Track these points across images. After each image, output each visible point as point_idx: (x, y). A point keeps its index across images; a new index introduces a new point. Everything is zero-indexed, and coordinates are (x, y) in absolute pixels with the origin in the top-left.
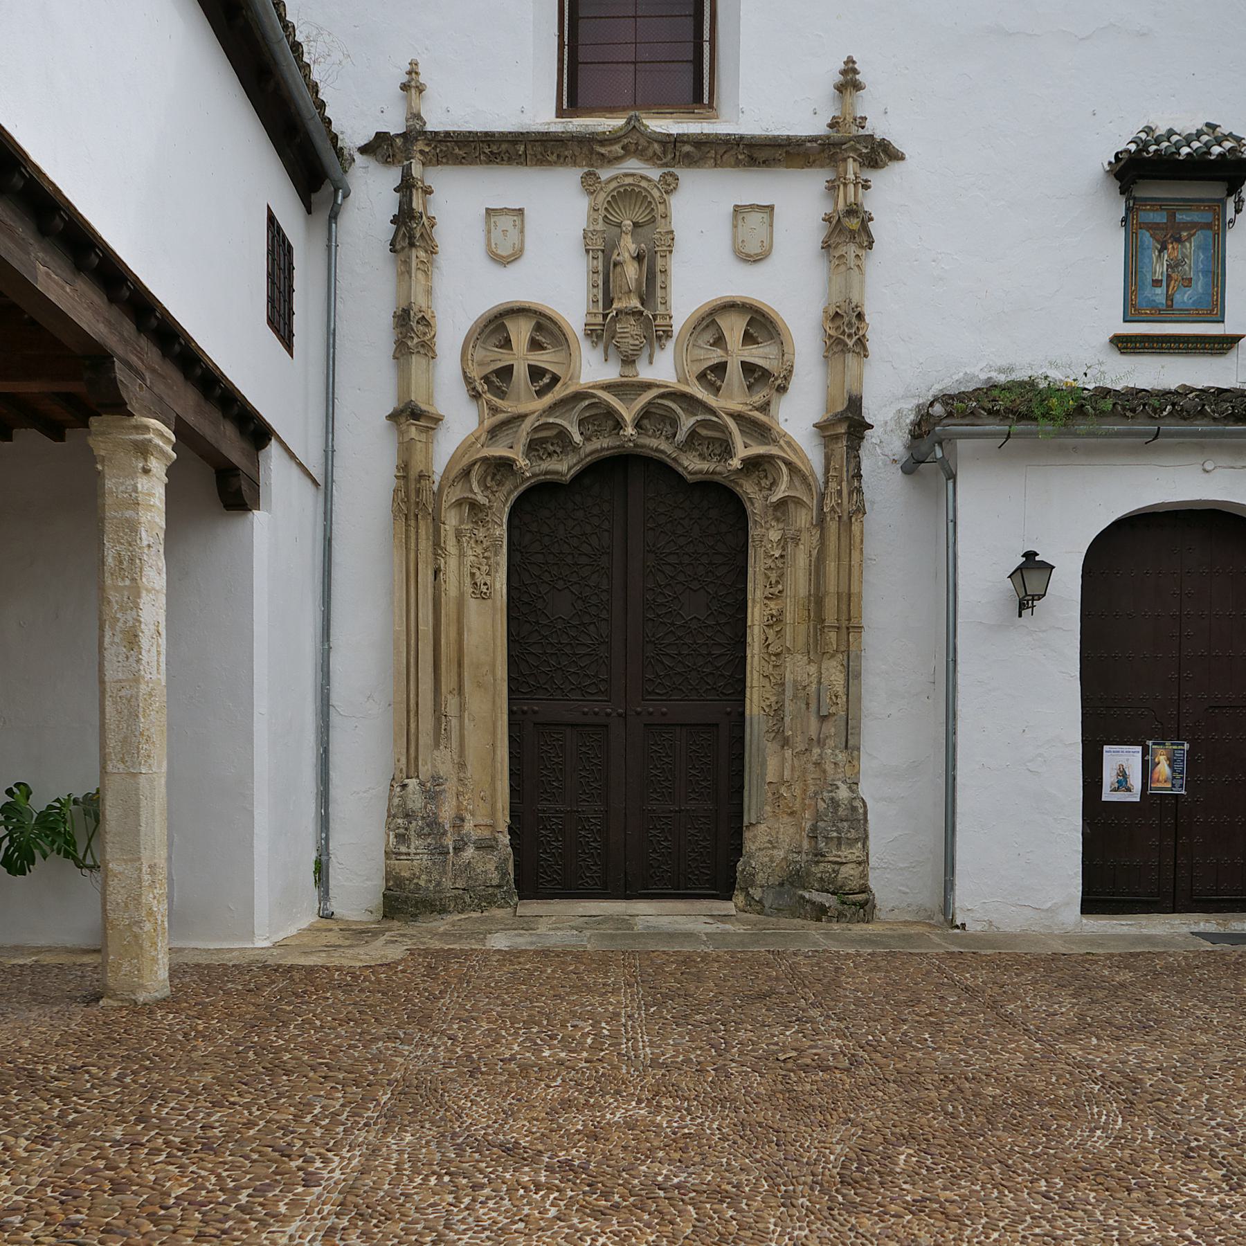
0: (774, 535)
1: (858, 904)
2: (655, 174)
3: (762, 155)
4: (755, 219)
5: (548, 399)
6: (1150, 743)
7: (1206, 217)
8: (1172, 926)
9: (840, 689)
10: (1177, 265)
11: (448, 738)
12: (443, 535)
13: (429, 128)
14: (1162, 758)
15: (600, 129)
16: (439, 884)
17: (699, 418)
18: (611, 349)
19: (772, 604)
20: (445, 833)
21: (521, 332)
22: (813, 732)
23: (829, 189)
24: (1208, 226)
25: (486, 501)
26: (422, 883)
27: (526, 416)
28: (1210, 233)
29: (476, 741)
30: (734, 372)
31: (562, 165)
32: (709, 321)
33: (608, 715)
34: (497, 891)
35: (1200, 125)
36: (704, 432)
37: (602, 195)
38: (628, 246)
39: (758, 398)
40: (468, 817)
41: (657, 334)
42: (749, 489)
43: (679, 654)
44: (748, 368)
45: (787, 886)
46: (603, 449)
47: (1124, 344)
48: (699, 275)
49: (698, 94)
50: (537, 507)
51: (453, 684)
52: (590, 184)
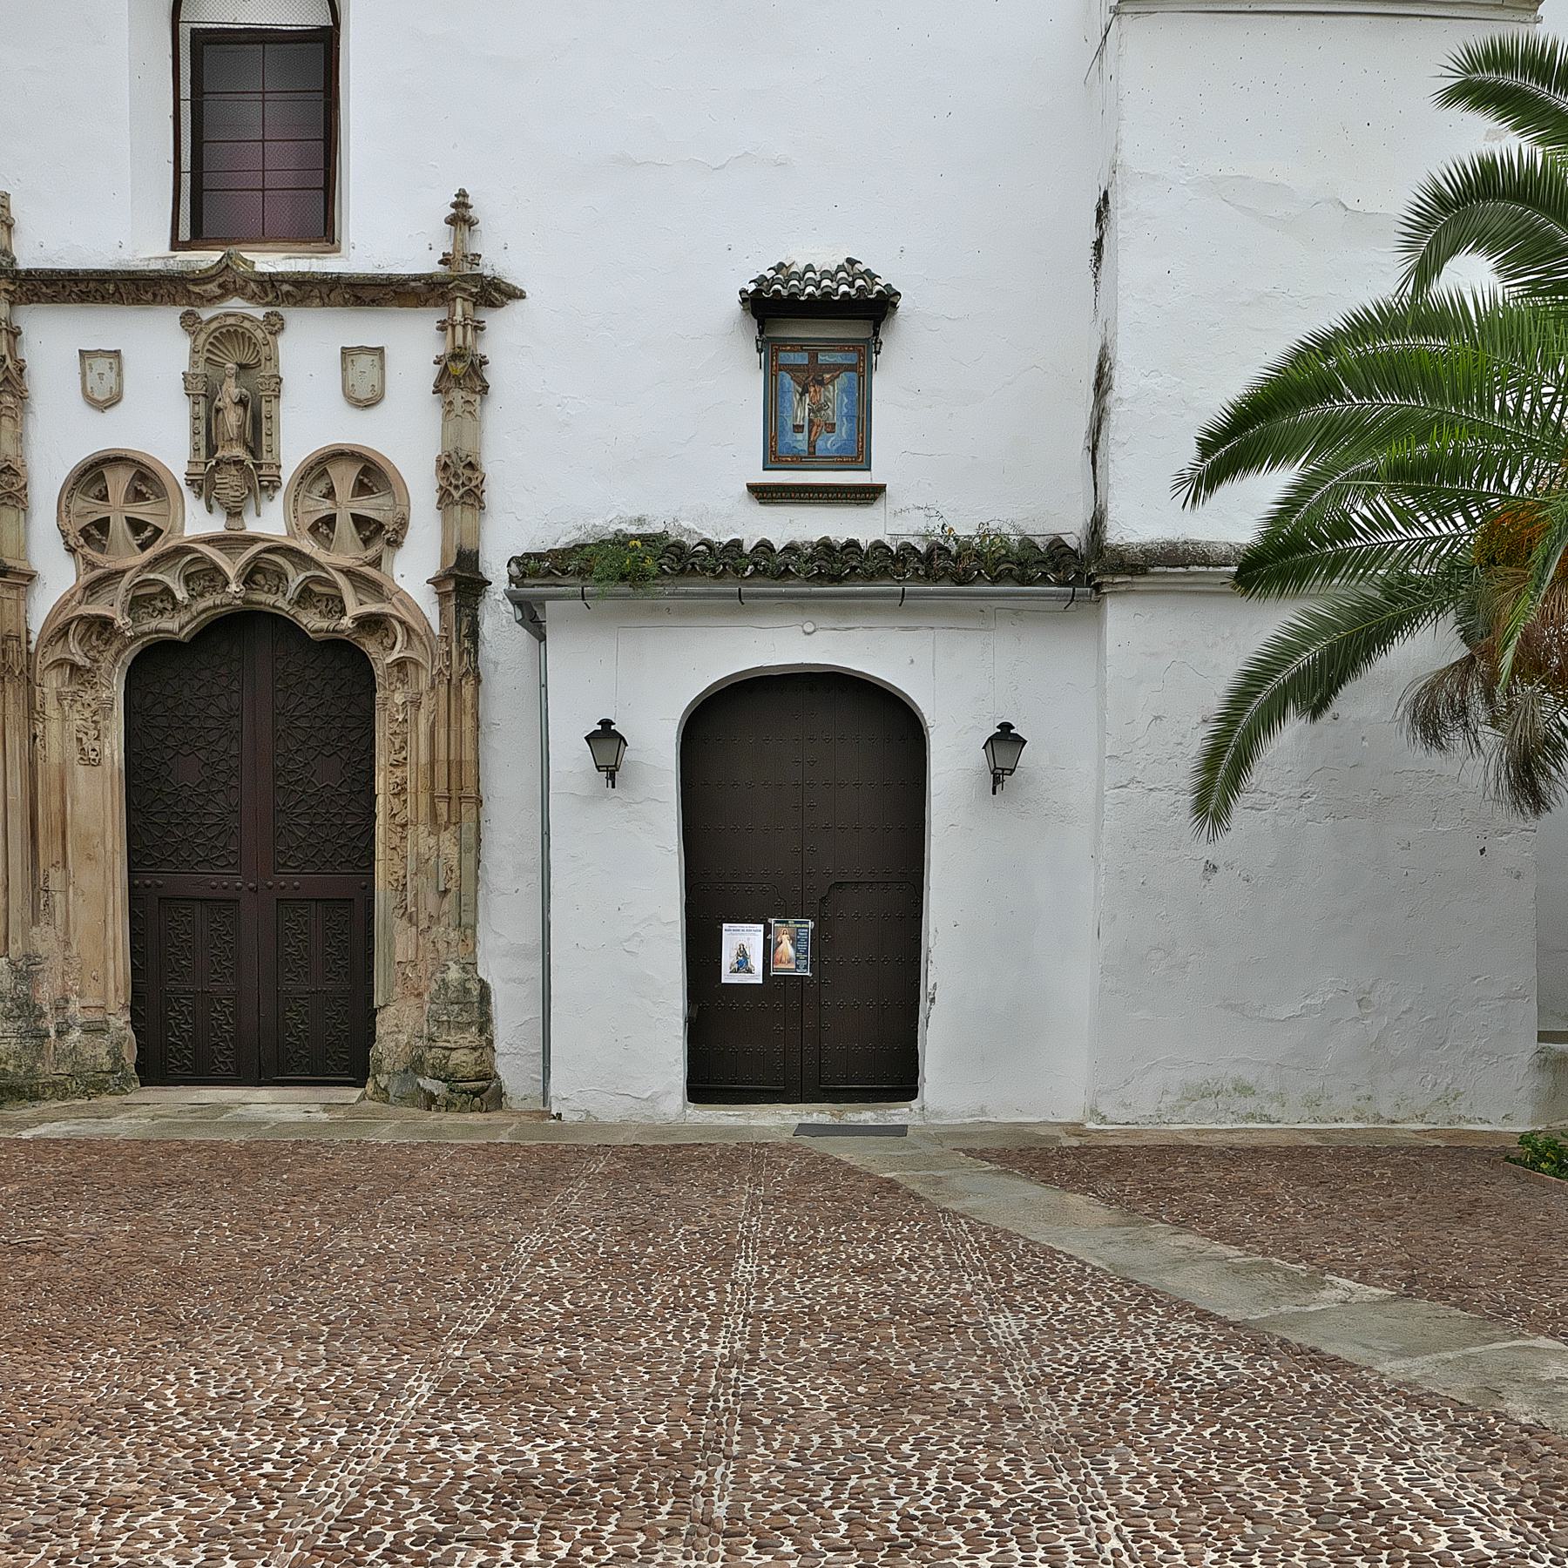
0: (399, 698)
1: (483, 1091)
2: (259, 313)
3: (366, 294)
4: (364, 361)
5: (150, 553)
6: (772, 921)
7: (851, 358)
8: (783, 1117)
9: (455, 863)
10: (819, 410)
11: (52, 915)
12: (38, 699)
13: (22, 265)
14: (785, 937)
15: (204, 266)
16: (31, 1069)
17: (308, 574)
18: (213, 501)
19: (398, 772)
20: (42, 1015)
21: (118, 481)
22: (432, 909)
23: (442, 329)
24: (850, 368)
25: (88, 663)
26: (10, 1069)
27: (124, 572)
28: (854, 375)
29: (84, 916)
30: (344, 525)
31: (161, 303)
32: (318, 468)
33: (238, 889)
34: (109, 1077)
35: (842, 261)
36: (317, 588)
37: (203, 336)
38: (231, 390)
39: (371, 553)
40: (74, 997)
41: (259, 481)
42: (371, 647)
43: (169, 823)
44: (359, 521)
45: (410, 1072)
46: (215, 607)
47: (763, 494)
48: (307, 422)
49: (323, 229)
50: (154, 664)
51: (57, 855)
52: (189, 322)
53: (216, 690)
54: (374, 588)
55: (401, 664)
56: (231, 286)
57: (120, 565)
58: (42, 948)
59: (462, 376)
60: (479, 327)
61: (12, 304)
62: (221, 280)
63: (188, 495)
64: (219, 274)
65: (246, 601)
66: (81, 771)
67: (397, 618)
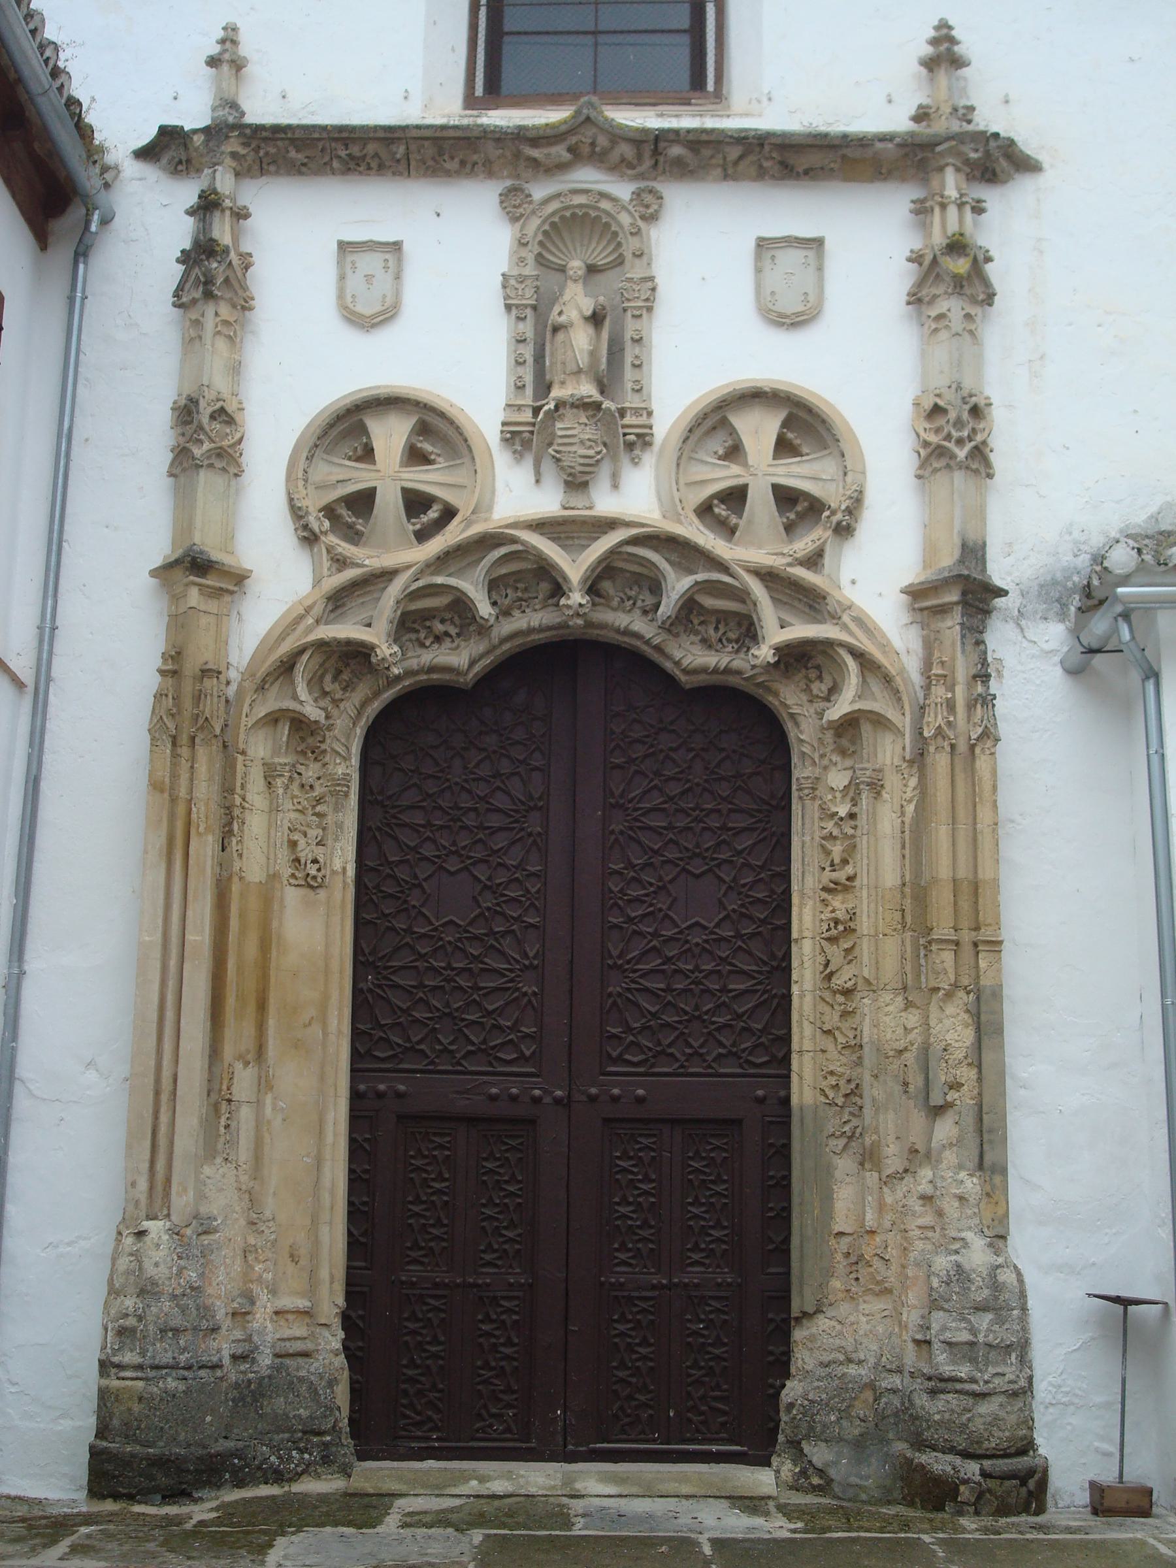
0: (838, 779)
2: (623, 190)
3: (802, 162)
11: (232, 1143)
13: (249, 119)
17: (700, 577)
19: (837, 902)
21: (390, 436)
30: (760, 502)
32: (715, 421)
33: (537, 1101)
36: (709, 602)
38: (576, 302)
42: (790, 698)
44: (785, 497)
52: (513, 205)
53: (505, 767)
54: (810, 601)
55: (849, 725)
56: (586, 150)
57: (388, 560)
58: (213, 1207)
59: (953, 280)
60: (978, 209)
61: (237, 175)
62: (573, 140)
63: (501, 459)
64: (571, 131)
65: (590, 624)
66: (292, 896)
67: (842, 644)
